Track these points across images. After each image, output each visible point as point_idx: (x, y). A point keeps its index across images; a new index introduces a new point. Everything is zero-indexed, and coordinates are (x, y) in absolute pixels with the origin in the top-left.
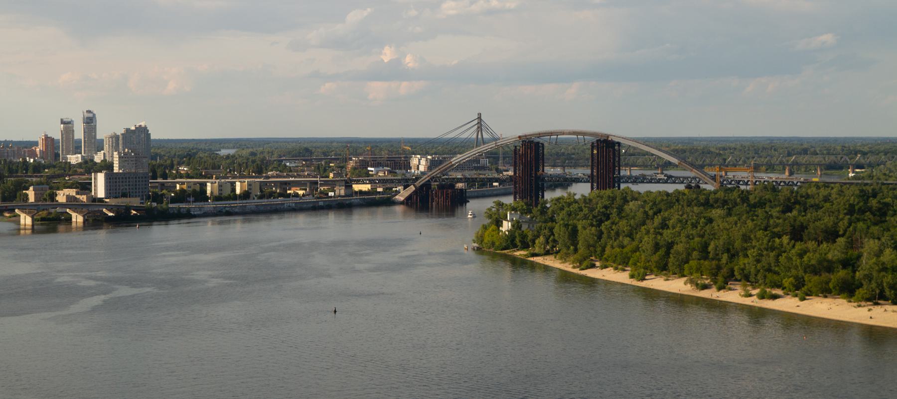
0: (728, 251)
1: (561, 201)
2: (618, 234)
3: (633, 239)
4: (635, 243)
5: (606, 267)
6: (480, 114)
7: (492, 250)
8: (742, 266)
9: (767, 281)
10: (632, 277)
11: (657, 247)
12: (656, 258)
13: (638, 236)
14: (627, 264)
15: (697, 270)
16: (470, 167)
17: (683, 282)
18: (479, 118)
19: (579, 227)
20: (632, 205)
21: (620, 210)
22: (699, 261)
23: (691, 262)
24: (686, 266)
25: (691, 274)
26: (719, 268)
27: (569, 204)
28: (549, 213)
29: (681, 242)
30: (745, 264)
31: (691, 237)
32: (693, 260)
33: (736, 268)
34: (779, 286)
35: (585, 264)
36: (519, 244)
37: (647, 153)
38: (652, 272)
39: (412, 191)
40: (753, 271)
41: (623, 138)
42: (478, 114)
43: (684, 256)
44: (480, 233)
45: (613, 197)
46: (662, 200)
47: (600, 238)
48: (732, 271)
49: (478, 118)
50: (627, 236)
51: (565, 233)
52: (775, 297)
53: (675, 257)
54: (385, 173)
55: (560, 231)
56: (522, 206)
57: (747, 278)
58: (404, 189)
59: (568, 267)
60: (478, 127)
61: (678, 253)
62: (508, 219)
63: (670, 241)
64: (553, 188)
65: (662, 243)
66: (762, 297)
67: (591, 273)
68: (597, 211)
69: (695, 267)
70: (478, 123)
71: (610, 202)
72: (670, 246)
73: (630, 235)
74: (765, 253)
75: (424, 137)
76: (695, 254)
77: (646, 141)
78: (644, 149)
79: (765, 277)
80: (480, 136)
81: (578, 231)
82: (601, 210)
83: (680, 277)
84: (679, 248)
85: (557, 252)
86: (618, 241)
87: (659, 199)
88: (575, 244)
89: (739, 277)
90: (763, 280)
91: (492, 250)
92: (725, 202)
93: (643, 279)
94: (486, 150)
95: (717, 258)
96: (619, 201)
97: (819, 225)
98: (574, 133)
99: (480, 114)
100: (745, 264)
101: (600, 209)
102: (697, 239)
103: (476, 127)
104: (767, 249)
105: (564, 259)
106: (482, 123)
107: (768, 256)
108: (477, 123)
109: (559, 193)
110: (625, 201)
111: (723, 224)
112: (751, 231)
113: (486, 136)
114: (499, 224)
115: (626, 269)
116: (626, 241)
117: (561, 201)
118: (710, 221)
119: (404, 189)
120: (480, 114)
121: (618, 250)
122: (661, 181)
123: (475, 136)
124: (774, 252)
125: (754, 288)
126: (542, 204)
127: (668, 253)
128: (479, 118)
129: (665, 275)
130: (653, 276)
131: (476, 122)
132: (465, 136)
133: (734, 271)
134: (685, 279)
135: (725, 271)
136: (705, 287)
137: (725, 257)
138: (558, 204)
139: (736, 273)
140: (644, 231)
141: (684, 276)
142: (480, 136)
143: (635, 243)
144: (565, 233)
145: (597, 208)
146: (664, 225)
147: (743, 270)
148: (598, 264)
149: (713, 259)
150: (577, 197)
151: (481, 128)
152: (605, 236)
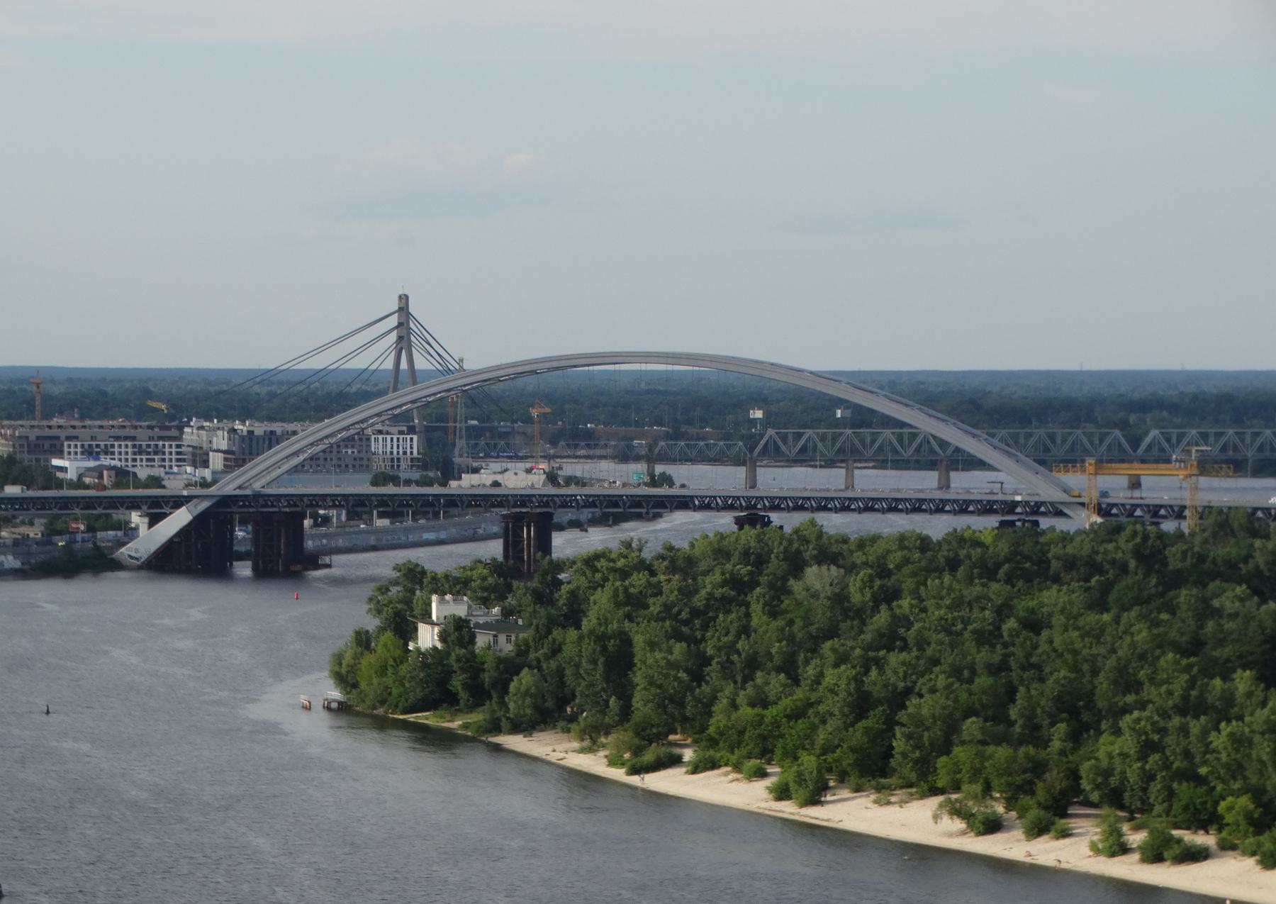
0: (1074, 713)
1: (601, 564)
2: (753, 664)
3: (797, 682)
4: (799, 694)
5: (712, 765)
6: (404, 299)
7: (380, 711)
8: (1105, 763)
9: (1177, 806)
10: (782, 793)
11: (861, 705)
12: (857, 735)
13: (811, 671)
14: (766, 753)
15: (974, 775)
16: (362, 459)
17: (929, 814)
18: (404, 309)
19: (638, 640)
20: (817, 577)
21: (779, 590)
22: (980, 748)
23: (957, 750)
24: (944, 759)
25: (957, 787)
26: (1038, 768)
27: (624, 574)
28: (561, 602)
29: (933, 691)
30: (1110, 756)
31: (966, 673)
32: (963, 743)
33: (1085, 768)
34: (1205, 819)
35: (649, 756)
36: (463, 695)
37: (888, 422)
38: (842, 778)
39: (102, 533)
40: (1133, 777)
41: (811, 373)
42: (400, 296)
43: (938, 732)
44: (348, 658)
45: (759, 556)
46: (906, 561)
47: (698, 677)
48: (1075, 776)
49: (401, 309)
50: (779, 670)
51: (595, 662)
52: (1195, 855)
53: (909, 737)
54: (101, 477)
55: (580, 656)
56: (484, 579)
57: (1115, 798)
58: (151, 525)
59: (595, 764)
60: (400, 338)
61: (919, 722)
62: (434, 617)
63: (901, 685)
64: (610, 523)
65: (877, 691)
66: (1154, 855)
67: (660, 781)
68: (703, 593)
69: (968, 766)
70: (400, 325)
71: (749, 568)
72: (898, 700)
73: (789, 668)
74: (1176, 721)
75: (257, 367)
76: (971, 726)
77: (860, 380)
78: (851, 399)
79: (1171, 794)
80: (404, 365)
81: (632, 655)
82: (718, 593)
83: (923, 796)
84: (924, 706)
85: (573, 719)
86: (749, 685)
87: (898, 556)
88: (625, 696)
89: (1095, 797)
90: (1166, 804)
91: (380, 711)
92: (1095, 567)
93: (814, 800)
94: (400, 406)
95: (1035, 735)
96: (775, 565)
97: (1038, 658)
98: (1116, 474)
99: (404, 299)
100: (1110, 756)
101: (714, 587)
102: (982, 681)
103: (393, 337)
104: (1183, 711)
105: (592, 737)
106: (412, 325)
107: (1184, 730)
108: (396, 324)
109: (597, 539)
110: (796, 565)
111: (1066, 635)
112: (1142, 657)
113: (421, 363)
114: (403, 628)
115: (770, 770)
116: (776, 682)
117: (601, 564)
118: (1034, 625)
119: (151, 525)
120: (407, 297)
121: (747, 712)
122: (971, 508)
123: (389, 364)
124: (1202, 718)
125: (1137, 828)
126: (546, 572)
127: (890, 723)
128: (404, 309)
129: (879, 789)
130: (845, 793)
131: (393, 321)
132: (359, 363)
133: (1081, 778)
134: (934, 802)
135: (1054, 779)
136: (992, 826)
137: (1058, 734)
138: (589, 573)
139: (1085, 785)
140: (831, 657)
141: (934, 791)
142: (404, 365)
143: (799, 694)
144: (595, 662)
145: (705, 587)
146: (891, 639)
147: (1107, 773)
148: (688, 755)
149: (1021, 742)
150: (647, 554)
151: (410, 341)
152: (713, 670)
